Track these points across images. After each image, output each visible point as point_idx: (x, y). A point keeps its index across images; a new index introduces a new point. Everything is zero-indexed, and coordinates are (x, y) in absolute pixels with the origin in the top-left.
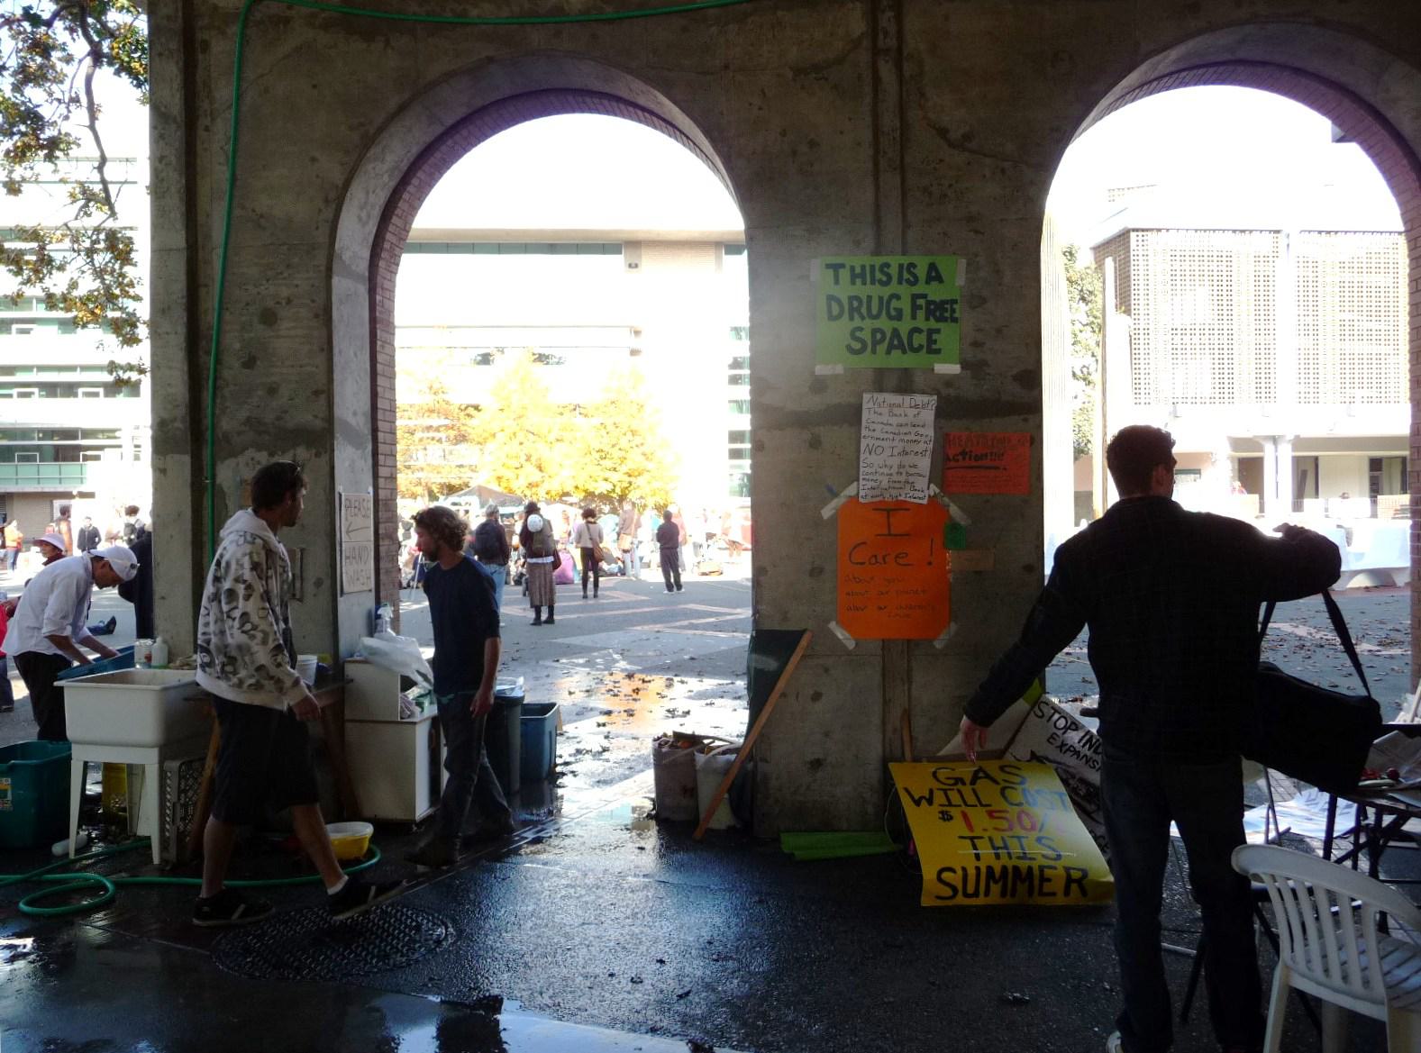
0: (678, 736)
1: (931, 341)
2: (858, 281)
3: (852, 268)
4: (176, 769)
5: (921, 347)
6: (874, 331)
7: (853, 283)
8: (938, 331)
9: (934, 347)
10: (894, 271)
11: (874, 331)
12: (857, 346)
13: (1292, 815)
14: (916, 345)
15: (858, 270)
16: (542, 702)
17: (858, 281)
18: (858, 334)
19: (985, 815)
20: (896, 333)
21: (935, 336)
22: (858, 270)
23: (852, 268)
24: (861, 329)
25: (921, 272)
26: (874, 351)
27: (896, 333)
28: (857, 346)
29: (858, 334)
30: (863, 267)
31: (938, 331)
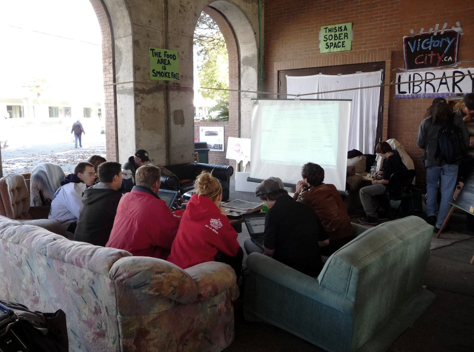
0: (247, 253)
1: (343, 44)
2: (330, 32)
3: (329, 29)
4: (107, 50)
5: (340, 46)
6: (331, 43)
7: (329, 32)
8: (344, 42)
9: (344, 46)
10: (337, 29)
11: (331, 43)
12: (326, 39)
13: (370, 254)
14: (339, 46)
15: (330, 29)
16: (132, 46)
17: (330, 32)
18: (326, 37)
19: (463, 91)
20: (335, 43)
21: (344, 43)
22: (330, 29)
23: (329, 29)
24: (326, 35)
25: (343, 28)
26: (330, 48)
27: (335, 43)
28: (326, 39)
29: (326, 37)
30: (331, 29)
31: (344, 42)
